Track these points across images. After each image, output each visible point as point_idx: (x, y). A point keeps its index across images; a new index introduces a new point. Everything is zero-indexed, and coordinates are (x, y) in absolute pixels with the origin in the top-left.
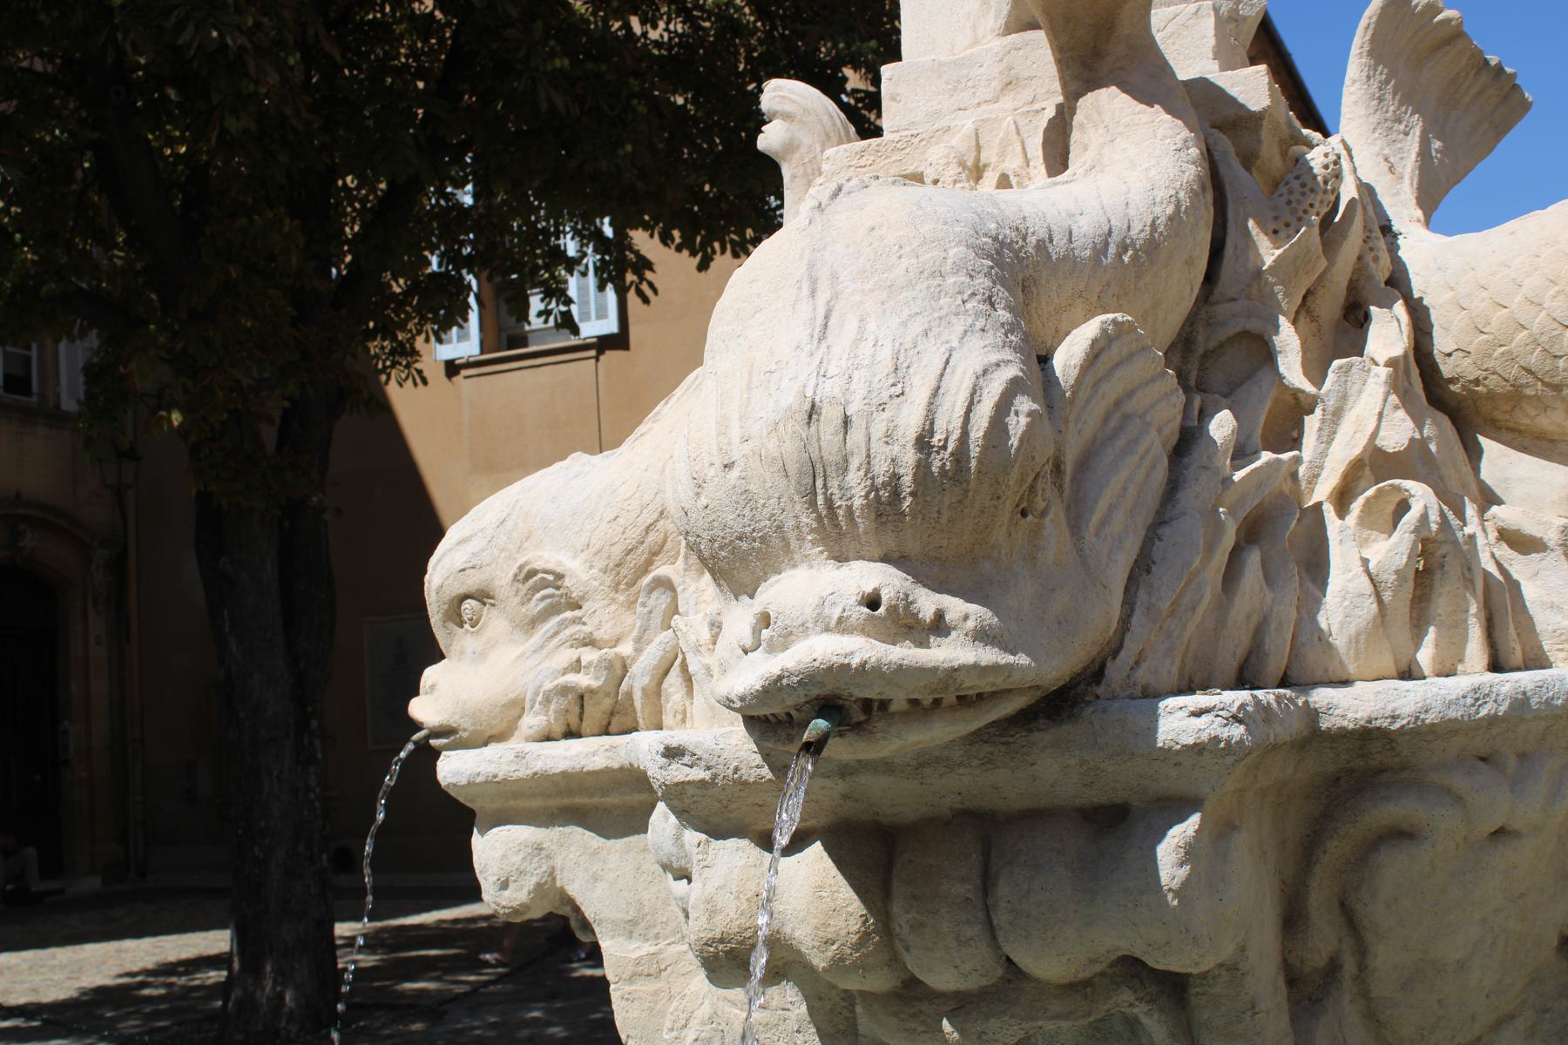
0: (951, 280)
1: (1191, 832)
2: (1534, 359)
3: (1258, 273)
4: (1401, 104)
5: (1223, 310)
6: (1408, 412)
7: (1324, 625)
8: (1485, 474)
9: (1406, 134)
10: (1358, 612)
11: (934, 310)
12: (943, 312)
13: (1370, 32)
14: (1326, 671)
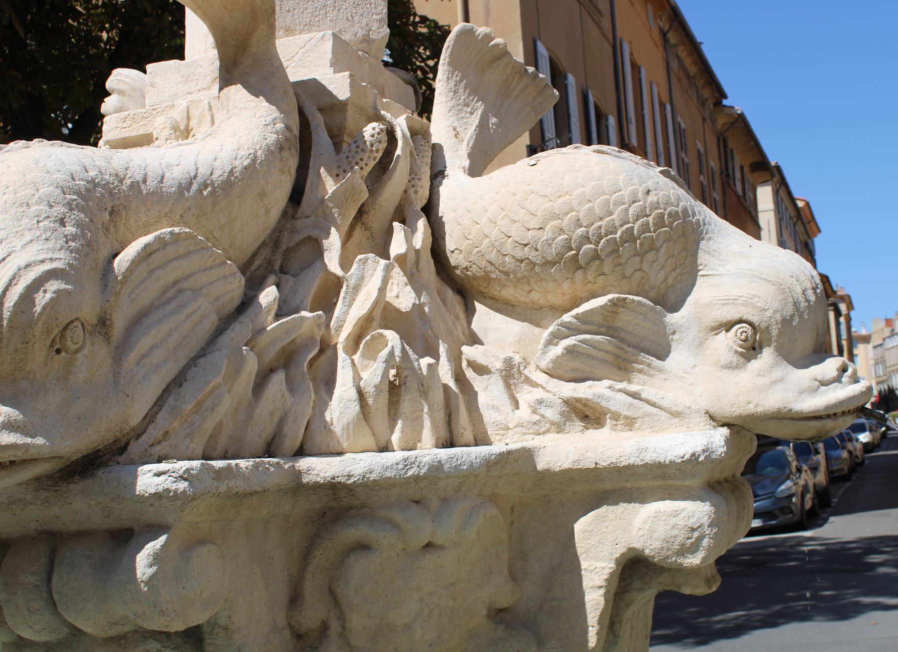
0: (33, 208)
1: (158, 546)
2: (493, 256)
3: (322, 201)
4: (470, 95)
5: (301, 223)
6: (413, 288)
7: (328, 419)
8: (475, 326)
9: (472, 113)
10: (348, 411)
11: (15, 227)
12: (21, 228)
13: (449, 51)
14: (328, 446)
